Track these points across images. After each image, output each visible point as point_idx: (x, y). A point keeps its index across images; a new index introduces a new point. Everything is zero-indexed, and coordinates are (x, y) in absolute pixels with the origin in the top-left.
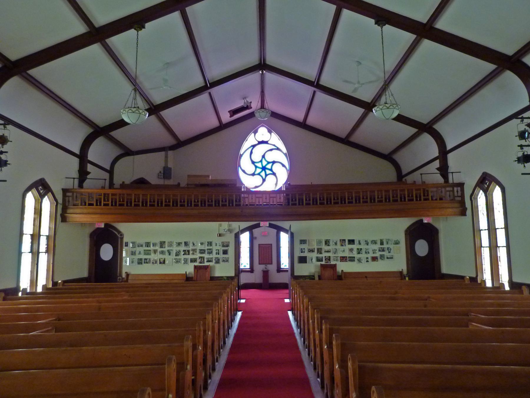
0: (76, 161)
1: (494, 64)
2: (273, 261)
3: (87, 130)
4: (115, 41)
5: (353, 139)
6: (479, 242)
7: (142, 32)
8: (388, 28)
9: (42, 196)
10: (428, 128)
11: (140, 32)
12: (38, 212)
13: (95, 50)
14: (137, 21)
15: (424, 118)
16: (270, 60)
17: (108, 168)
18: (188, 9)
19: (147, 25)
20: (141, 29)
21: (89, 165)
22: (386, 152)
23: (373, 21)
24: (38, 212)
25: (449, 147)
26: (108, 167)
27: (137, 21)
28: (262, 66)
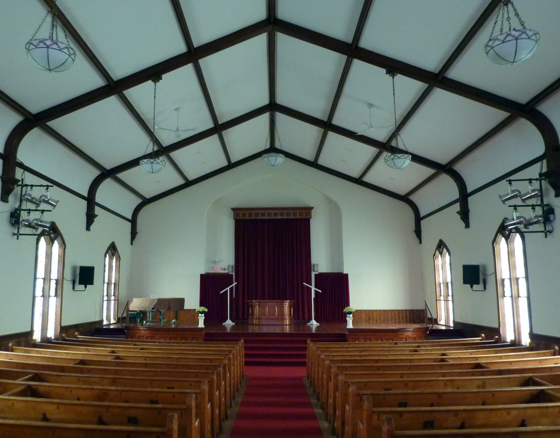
0: (84, 204)
1: (508, 112)
2: (49, 327)
3: (96, 173)
4: (132, 93)
5: (366, 179)
6: (516, 292)
7: (160, 84)
8: (400, 78)
9: (52, 241)
10: (447, 169)
11: (157, 84)
12: (49, 256)
13: (112, 101)
14: (154, 73)
15: (443, 159)
16: (281, 100)
17: (130, 218)
18: (201, 62)
19: (164, 76)
20: (158, 81)
21: (96, 207)
22: (403, 192)
23: (384, 71)
24: (49, 256)
25: (469, 190)
26: (130, 217)
27: (154, 73)
28: (273, 107)
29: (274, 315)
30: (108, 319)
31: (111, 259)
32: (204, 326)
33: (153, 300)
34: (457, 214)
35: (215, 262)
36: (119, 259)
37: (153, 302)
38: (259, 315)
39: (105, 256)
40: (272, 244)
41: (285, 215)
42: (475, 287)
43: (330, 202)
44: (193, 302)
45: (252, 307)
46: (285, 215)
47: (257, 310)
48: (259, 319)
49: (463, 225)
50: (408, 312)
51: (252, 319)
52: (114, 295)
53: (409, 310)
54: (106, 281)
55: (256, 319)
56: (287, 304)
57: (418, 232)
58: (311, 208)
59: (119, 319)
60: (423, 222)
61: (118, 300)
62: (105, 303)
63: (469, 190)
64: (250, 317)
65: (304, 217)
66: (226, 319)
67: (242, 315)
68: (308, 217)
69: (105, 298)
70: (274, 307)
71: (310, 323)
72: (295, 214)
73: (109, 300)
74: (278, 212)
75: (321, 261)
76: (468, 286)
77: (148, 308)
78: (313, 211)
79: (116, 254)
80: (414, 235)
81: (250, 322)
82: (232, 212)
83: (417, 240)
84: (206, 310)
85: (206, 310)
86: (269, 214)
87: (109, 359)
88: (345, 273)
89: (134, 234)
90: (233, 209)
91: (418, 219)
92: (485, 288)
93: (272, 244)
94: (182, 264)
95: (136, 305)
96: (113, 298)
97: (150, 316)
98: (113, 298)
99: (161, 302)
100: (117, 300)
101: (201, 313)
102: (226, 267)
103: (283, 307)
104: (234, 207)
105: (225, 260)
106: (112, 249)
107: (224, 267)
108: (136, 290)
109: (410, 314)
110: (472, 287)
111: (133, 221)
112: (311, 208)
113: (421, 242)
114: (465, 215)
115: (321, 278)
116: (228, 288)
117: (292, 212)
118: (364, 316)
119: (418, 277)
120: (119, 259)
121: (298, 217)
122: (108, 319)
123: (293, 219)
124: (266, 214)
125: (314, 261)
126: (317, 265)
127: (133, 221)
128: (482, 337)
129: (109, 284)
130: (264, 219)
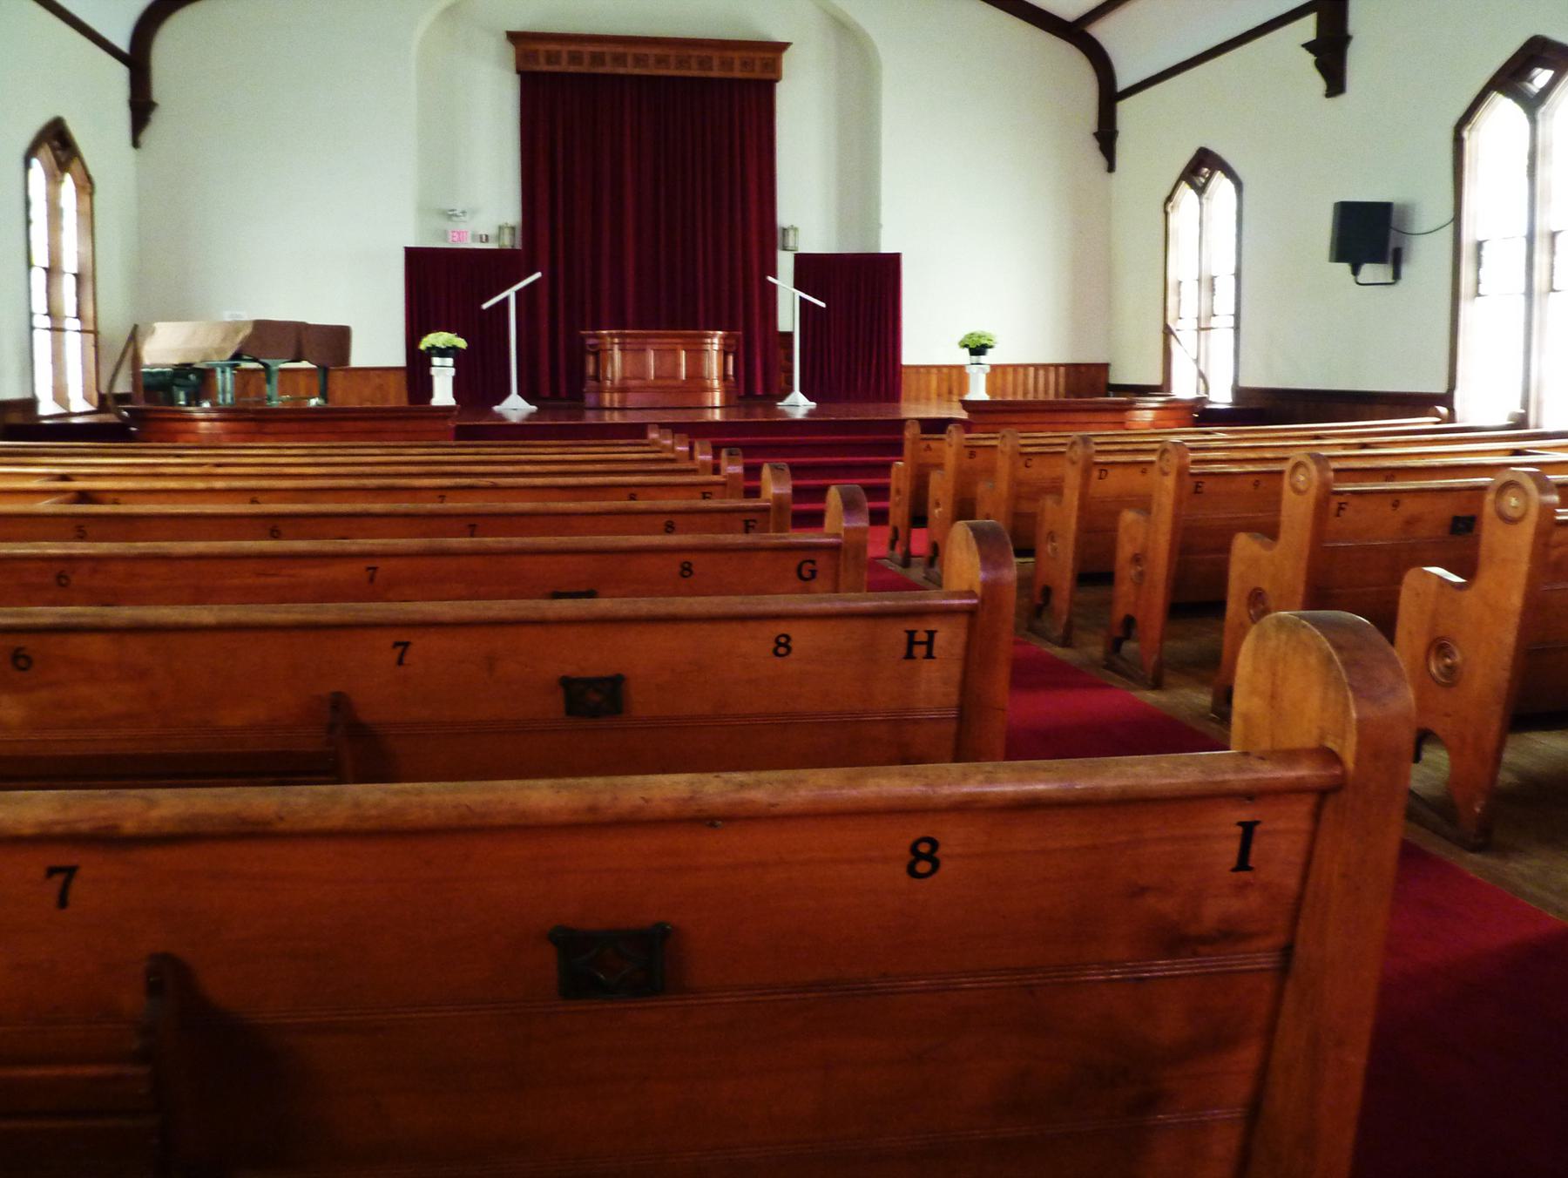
29: (675, 376)
30: (60, 395)
31: (54, 180)
32: (451, 402)
33: (235, 327)
34: (1303, 50)
35: (450, 215)
36: (86, 186)
37: (237, 332)
38: (624, 378)
39: (27, 165)
40: (644, 168)
41: (694, 64)
42: (1369, 271)
43: (844, 32)
44: (379, 343)
45: (596, 354)
46: (694, 64)
47: (617, 363)
48: (623, 390)
49: (1319, 83)
50: (1062, 370)
51: (600, 391)
52: (79, 316)
53: (1066, 366)
54: (41, 258)
55: (613, 390)
56: (715, 342)
57: (1106, 137)
58: (782, 47)
59: (102, 398)
60: (1125, 109)
61: (95, 333)
62: (43, 340)
63: (1122, 83)
64: (591, 383)
65: (757, 74)
66: (507, 393)
67: (561, 380)
68: (768, 76)
69: (41, 321)
70: (675, 352)
71: (789, 400)
72: (727, 64)
73: (57, 330)
74: (672, 52)
75: (808, 216)
76: (1345, 267)
77: (219, 351)
78: (786, 57)
79: (75, 166)
80: (1095, 144)
81: (590, 400)
82: (510, 52)
83: (1101, 161)
84: (462, 343)
85: (462, 343)
86: (639, 60)
87: (44, 506)
88: (884, 250)
89: (141, 109)
90: (514, 37)
91: (1109, 96)
92: (1397, 275)
93: (644, 168)
94: (346, 200)
95: (164, 347)
96: (72, 324)
97: (225, 381)
98: (72, 324)
99: (268, 337)
100: (92, 332)
101: (443, 353)
102: (492, 231)
103: (697, 354)
104: (517, 27)
105: (489, 211)
106: (56, 143)
107: (483, 232)
108: (164, 293)
109: (1067, 375)
110: (1355, 272)
111: (137, 60)
112: (782, 47)
113: (1111, 168)
114: (1331, 56)
115: (810, 270)
116: (511, 293)
117: (716, 57)
118: (934, 384)
119: (1092, 267)
120: (86, 186)
121: (738, 73)
122: (60, 395)
123: (721, 80)
124: (630, 60)
125: (785, 216)
126: (796, 229)
127: (137, 60)
128: (1438, 415)
129: (52, 272)
130: (622, 77)
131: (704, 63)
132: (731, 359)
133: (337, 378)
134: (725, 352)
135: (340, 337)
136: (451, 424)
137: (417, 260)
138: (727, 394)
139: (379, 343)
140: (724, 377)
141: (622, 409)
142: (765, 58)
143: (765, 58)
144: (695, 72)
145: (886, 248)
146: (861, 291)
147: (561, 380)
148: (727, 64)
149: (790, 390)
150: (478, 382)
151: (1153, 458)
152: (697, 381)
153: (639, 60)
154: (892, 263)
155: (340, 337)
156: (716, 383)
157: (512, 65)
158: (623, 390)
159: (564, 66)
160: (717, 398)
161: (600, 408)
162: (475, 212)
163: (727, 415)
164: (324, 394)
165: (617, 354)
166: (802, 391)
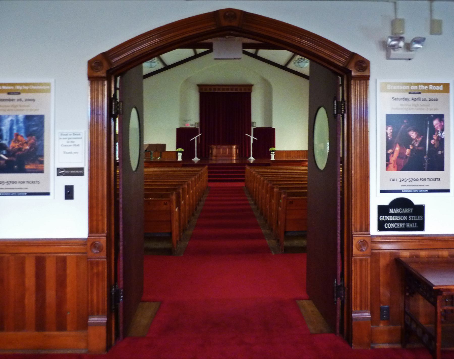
35: (186, 121)
44: (171, 146)
47: (215, 151)
48: (216, 156)
51: (212, 156)
55: (215, 156)
56: (234, 147)
58: (252, 86)
65: (247, 91)
66: (195, 157)
67: (204, 154)
71: (250, 158)
72: (236, 89)
75: (258, 120)
78: (253, 87)
81: (210, 158)
82: (197, 87)
90: (199, 85)
105: (193, 119)
112: (252, 86)
116: (196, 138)
123: (244, 93)
125: (253, 119)
131: (241, 89)
132: (238, 150)
133: (163, 153)
134: (236, 149)
135: (164, 146)
136: (181, 164)
137: (177, 129)
138: (237, 157)
139: (171, 146)
140: (236, 154)
141: (216, 160)
142: (249, 87)
143: (249, 87)
144: (234, 91)
145: (273, 127)
146: (267, 136)
147: (204, 154)
148: (206, 89)
149: (250, 156)
150: (188, 155)
151: (306, 186)
152: (231, 155)
153: (232, 89)
154: (274, 129)
155: (164, 146)
156: (235, 155)
157: (198, 91)
158: (216, 156)
159: (208, 91)
160: (235, 158)
161: (212, 160)
162: (190, 120)
163: (236, 162)
164: (161, 156)
165: (215, 150)
166: (253, 156)
